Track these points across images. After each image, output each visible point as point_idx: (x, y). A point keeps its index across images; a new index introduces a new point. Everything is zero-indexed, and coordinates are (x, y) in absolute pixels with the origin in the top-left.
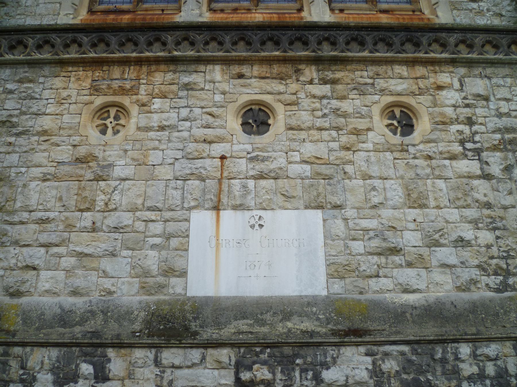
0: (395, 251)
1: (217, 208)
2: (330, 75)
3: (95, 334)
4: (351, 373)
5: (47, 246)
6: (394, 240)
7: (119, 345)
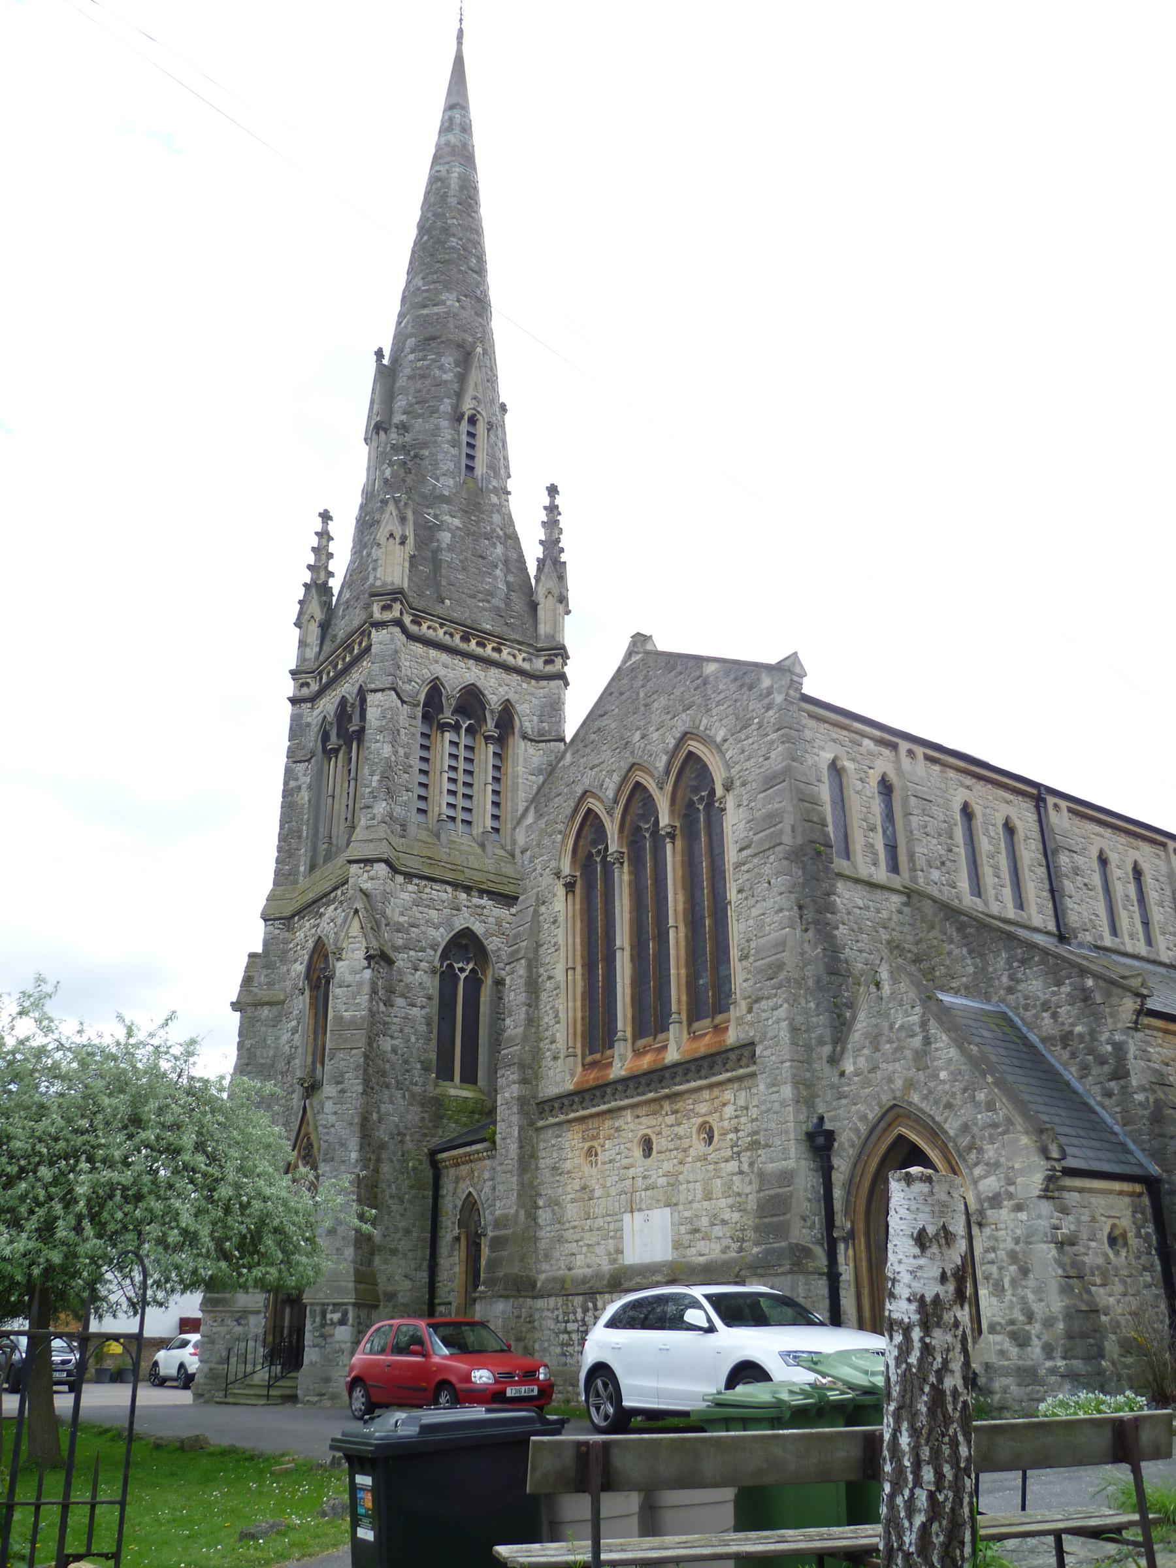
0: (697, 1231)
1: (632, 1212)
2: (675, 1107)
3: (591, 1288)
4: (415, 1234)
5: (577, 1241)
6: (697, 1224)
7: (600, 1293)
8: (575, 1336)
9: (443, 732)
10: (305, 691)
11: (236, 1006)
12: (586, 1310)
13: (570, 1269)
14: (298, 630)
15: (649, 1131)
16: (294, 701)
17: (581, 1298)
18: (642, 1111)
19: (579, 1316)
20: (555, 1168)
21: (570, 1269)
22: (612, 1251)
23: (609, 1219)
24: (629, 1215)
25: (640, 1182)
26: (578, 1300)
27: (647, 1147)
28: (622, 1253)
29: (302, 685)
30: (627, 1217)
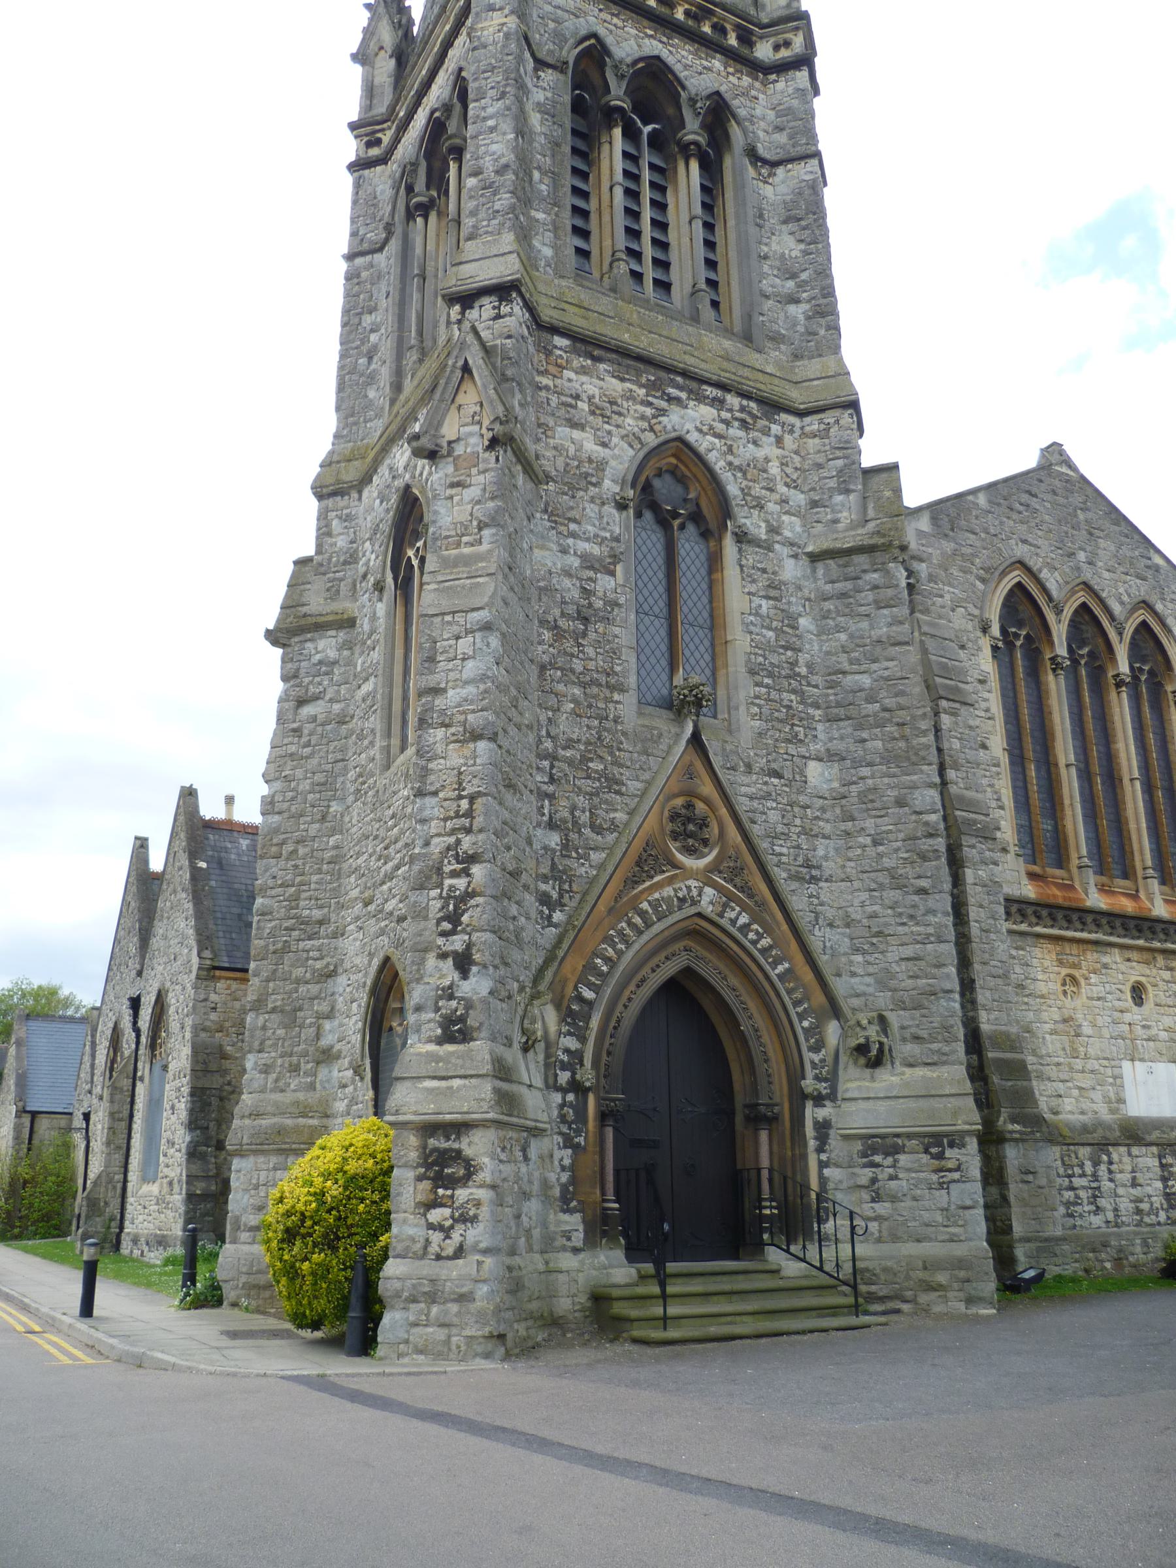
7: (1114, 1145)
8: (1083, 1194)
9: (757, 1130)
10: (375, 152)
11: (274, 637)
12: (1096, 1163)
13: (1056, 1113)
14: (358, 70)
15: (1143, 979)
16: (355, 167)
17: (1088, 1149)
18: (1135, 955)
19: (1089, 1168)
20: (1021, 987)
21: (1056, 1113)
22: (1113, 1099)
23: (1105, 1063)
24: (1129, 1063)
25: (1139, 1031)
26: (1084, 1152)
27: (1138, 993)
28: (1124, 1102)
29: (369, 145)
30: (1126, 1065)
